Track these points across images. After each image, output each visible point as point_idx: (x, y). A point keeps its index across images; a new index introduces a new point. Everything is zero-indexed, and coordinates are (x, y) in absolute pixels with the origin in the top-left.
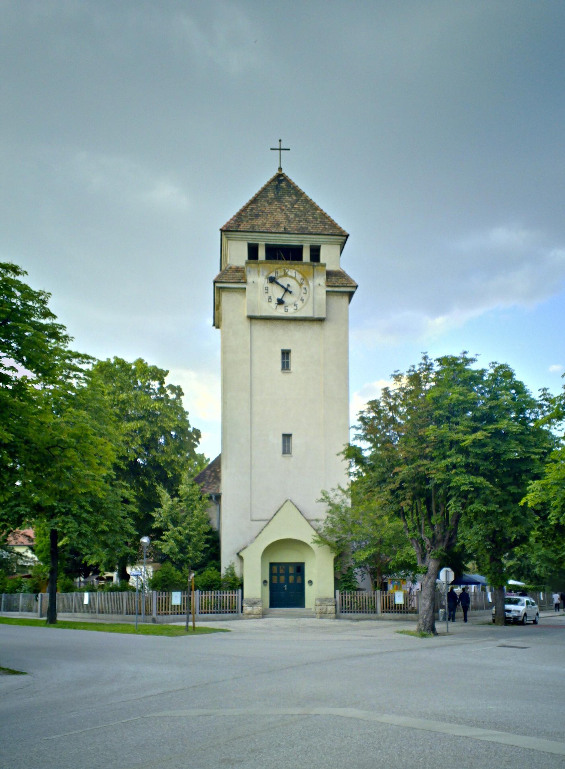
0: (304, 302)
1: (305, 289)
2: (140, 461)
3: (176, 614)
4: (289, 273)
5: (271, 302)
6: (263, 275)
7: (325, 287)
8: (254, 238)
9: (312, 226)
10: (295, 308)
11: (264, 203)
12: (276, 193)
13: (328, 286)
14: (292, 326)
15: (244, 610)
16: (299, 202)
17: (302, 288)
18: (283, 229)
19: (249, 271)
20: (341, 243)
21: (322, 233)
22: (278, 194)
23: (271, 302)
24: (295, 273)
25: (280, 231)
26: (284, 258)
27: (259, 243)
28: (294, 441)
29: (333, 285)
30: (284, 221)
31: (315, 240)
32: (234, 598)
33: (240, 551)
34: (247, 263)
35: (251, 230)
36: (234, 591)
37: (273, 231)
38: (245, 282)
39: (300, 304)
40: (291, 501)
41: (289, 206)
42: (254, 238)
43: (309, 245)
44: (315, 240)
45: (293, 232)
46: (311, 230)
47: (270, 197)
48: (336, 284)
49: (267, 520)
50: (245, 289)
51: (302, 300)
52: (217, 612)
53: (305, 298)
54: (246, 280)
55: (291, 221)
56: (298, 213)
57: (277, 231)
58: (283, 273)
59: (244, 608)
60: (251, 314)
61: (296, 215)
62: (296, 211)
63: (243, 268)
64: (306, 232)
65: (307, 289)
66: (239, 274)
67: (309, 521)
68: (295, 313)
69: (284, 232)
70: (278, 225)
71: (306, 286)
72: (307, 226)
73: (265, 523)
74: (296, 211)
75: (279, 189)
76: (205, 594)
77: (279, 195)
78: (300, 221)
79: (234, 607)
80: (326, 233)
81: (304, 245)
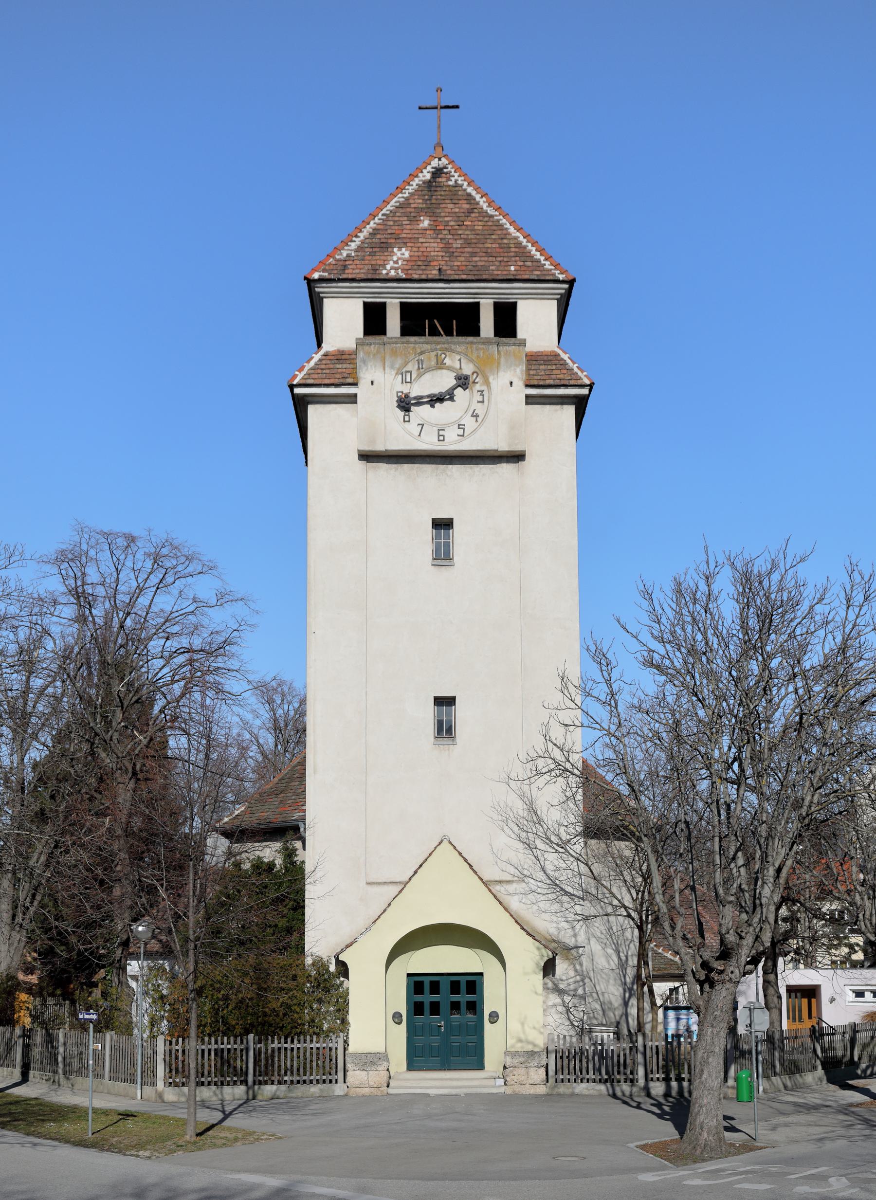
0: (479, 419)
1: (481, 392)
2: (669, 768)
3: (328, 1081)
4: (447, 361)
5: (409, 421)
6: (392, 367)
7: (523, 387)
8: (374, 292)
9: (497, 263)
10: (461, 432)
11: (401, 219)
12: (426, 197)
13: (528, 386)
14: (455, 470)
15: (348, 1079)
16: (473, 215)
17: (475, 392)
18: (436, 272)
19: (364, 362)
20: (559, 297)
21: (518, 277)
22: (430, 200)
23: (409, 421)
24: (460, 360)
25: (430, 277)
26: (442, 333)
27: (388, 301)
28: (462, 713)
29: (541, 383)
30: (440, 254)
31: (506, 291)
32: (302, 1051)
33: (342, 951)
34: (359, 343)
35: (370, 276)
36: (232, 1039)
37: (416, 277)
38: (355, 384)
39: (469, 423)
40: (450, 843)
41: (452, 223)
42: (374, 292)
43: (492, 301)
44: (506, 291)
45: (457, 277)
46: (496, 272)
47: (413, 206)
48: (548, 382)
49: (400, 882)
50: (355, 395)
51: (475, 416)
52: (305, 1082)
53: (480, 410)
54: (356, 378)
55: (455, 254)
56: (470, 237)
57: (424, 277)
58: (433, 363)
59: (348, 1073)
60: (367, 447)
61: (468, 242)
62: (467, 232)
63: (354, 353)
64: (484, 277)
65: (486, 393)
66: (345, 366)
67: (485, 884)
68: (461, 441)
69: (437, 277)
70: (427, 263)
71: (484, 388)
72: (487, 264)
73: (395, 889)
74: (467, 232)
75: (433, 189)
76: (299, 1042)
77: (434, 201)
78: (474, 254)
79: (206, 1073)
80: (526, 277)
81: (482, 301)
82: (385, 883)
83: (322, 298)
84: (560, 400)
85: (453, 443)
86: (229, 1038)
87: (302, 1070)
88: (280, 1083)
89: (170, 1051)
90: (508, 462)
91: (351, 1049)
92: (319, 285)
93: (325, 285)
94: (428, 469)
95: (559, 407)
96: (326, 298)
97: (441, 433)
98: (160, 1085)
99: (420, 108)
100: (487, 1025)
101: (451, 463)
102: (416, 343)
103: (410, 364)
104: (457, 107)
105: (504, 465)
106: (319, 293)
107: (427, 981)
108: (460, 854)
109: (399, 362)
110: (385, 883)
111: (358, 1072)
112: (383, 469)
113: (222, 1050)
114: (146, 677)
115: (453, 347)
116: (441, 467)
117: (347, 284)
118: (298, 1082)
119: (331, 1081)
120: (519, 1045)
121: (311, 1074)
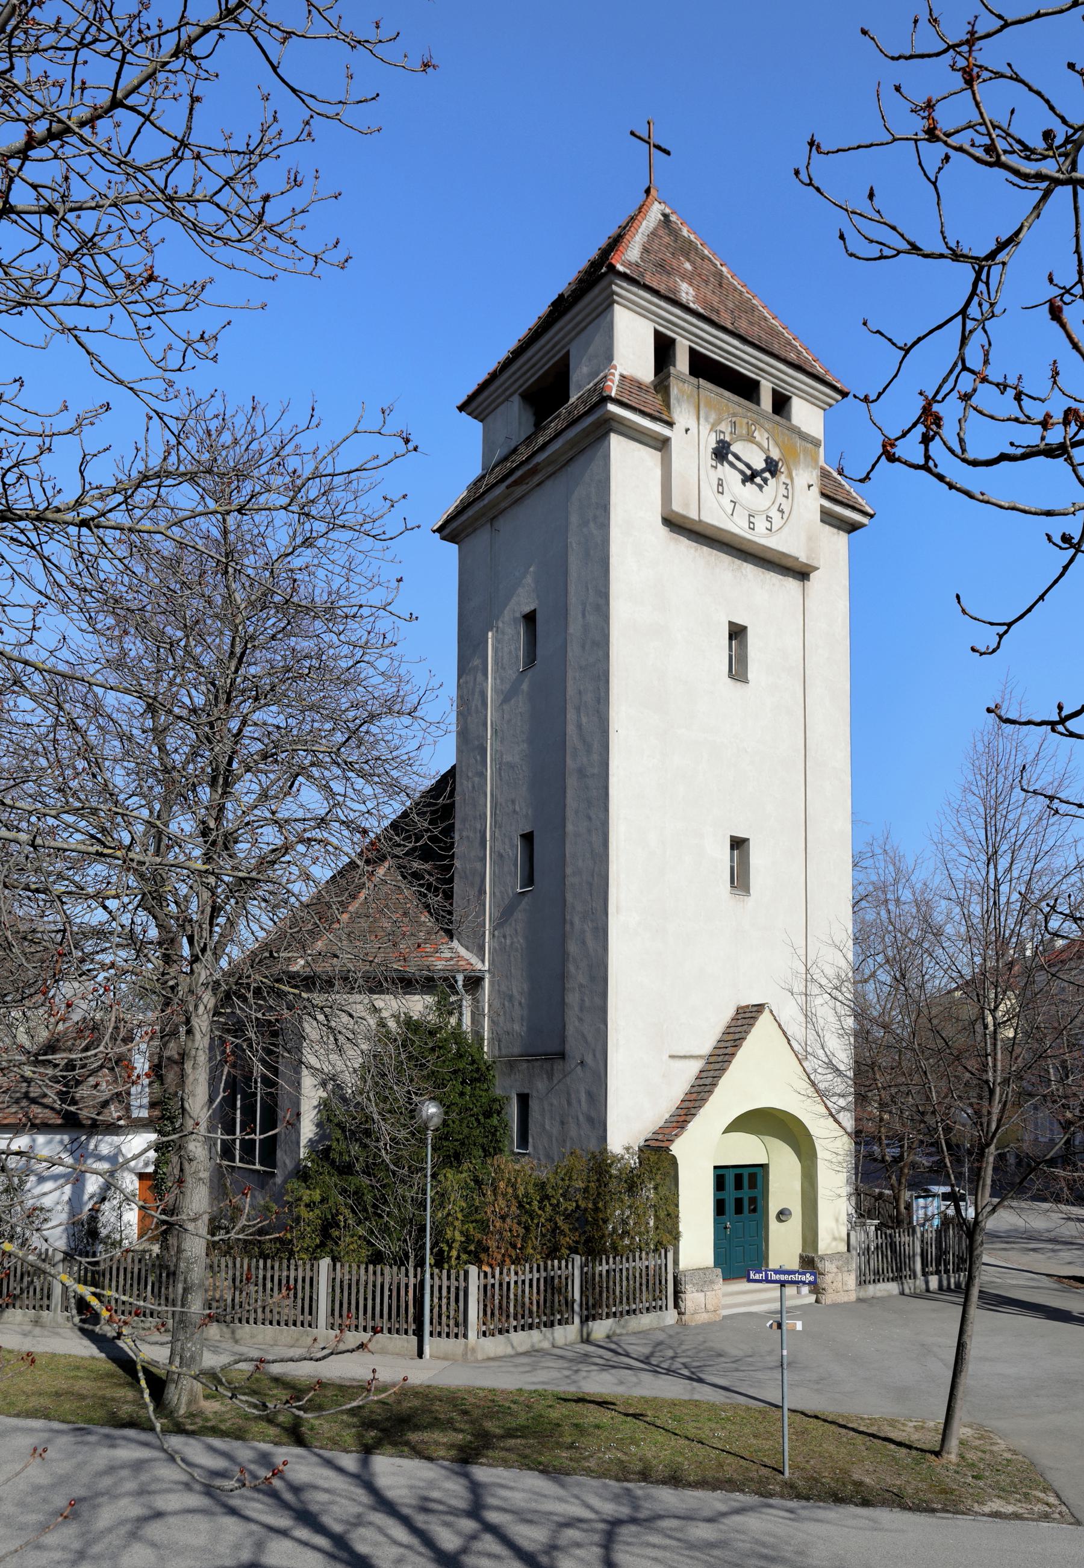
53: (786, 508)
71: (788, 481)
81: (763, 382)
82: (685, 1057)
83: (614, 302)
84: (838, 523)
85: (761, 537)
86: (560, 1262)
87: (631, 1300)
88: (608, 1316)
89: (485, 1286)
90: (794, 578)
91: (682, 1266)
92: (619, 282)
93: (625, 285)
94: (725, 559)
95: (835, 530)
96: (618, 303)
97: (752, 519)
98: (472, 1334)
99: (632, 133)
100: (773, 1224)
101: (746, 561)
102: (729, 400)
103: (723, 423)
104: (668, 153)
105: (791, 579)
106: (614, 293)
107: (746, 1173)
108: (780, 1026)
109: (713, 417)
110: (685, 1057)
111: (696, 1294)
112: (684, 546)
113: (553, 1278)
114: (135, 799)
115: (762, 421)
116: (738, 562)
117: (648, 296)
118: (628, 1312)
119: (661, 1308)
120: (834, 1244)
121: (628, 1304)
